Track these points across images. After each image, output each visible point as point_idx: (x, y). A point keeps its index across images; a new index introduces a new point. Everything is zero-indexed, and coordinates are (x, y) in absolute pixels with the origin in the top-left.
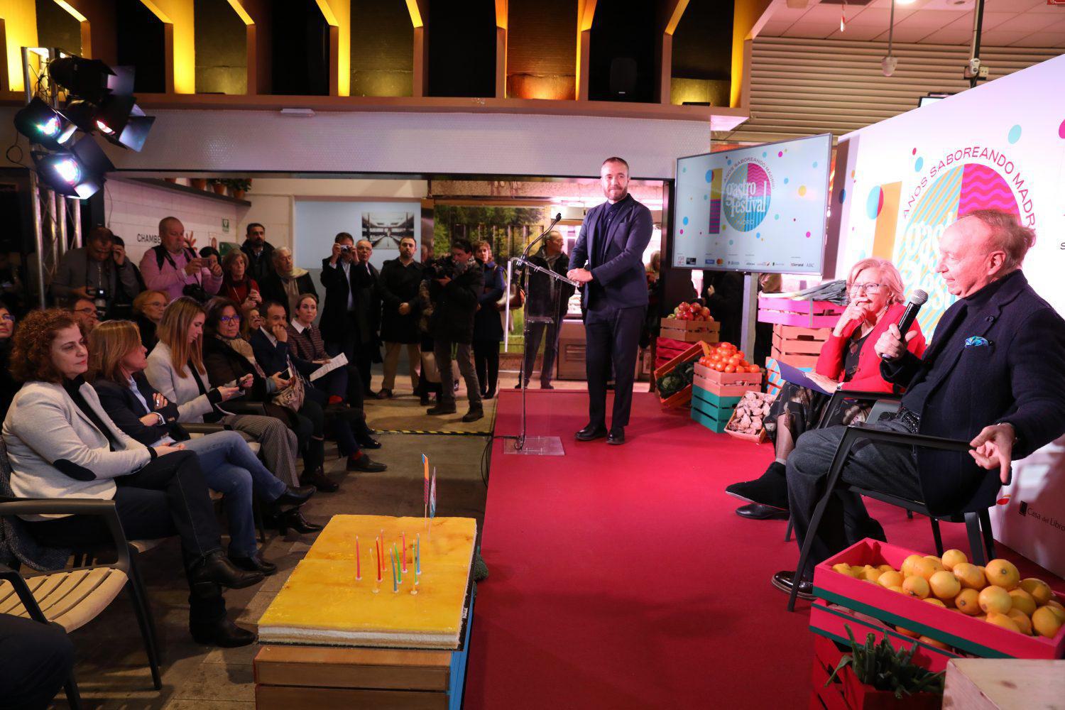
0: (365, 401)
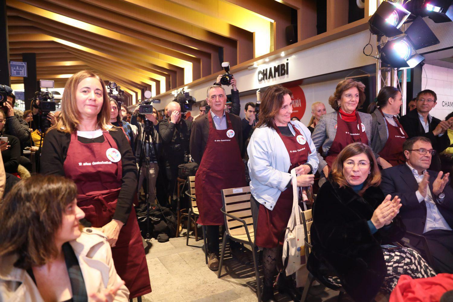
0: (139, 139)
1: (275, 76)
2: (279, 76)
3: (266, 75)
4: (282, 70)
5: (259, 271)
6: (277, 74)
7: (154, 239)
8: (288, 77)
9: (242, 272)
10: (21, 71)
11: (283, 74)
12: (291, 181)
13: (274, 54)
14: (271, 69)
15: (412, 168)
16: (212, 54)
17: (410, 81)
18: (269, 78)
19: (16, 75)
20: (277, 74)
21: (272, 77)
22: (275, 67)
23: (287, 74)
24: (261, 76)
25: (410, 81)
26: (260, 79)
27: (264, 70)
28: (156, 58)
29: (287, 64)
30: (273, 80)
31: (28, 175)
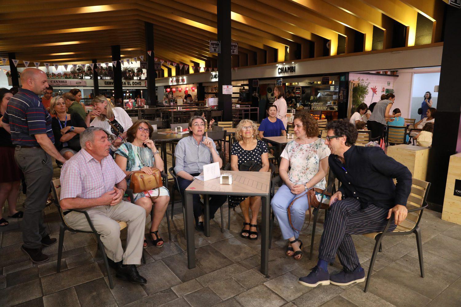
1: (288, 72)
2: (290, 72)
3: (282, 71)
4: (292, 69)
5: (142, 91)
6: (289, 71)
7: (146, 77)
8: (295, 73)
9: (131, 113)
10: (217, 48)
11: (292, 72)
12: (123, 65)
13: (286, 61)
14: (286, 68)
15: (168, 110)
16: (302, 46)
17: (223, 93)
18: (285, 72)
19: (140, 90)
20: (289, 71)
21: (286, 72)
22: (288, 67)
23: (295, 71)
24: (280, 71)
25: (223, 93)
26: (279, 72)
27: (282, 68)
28: (402, 3)
29: (295, 67)
30: (287, 74)
31: (337, 97)
